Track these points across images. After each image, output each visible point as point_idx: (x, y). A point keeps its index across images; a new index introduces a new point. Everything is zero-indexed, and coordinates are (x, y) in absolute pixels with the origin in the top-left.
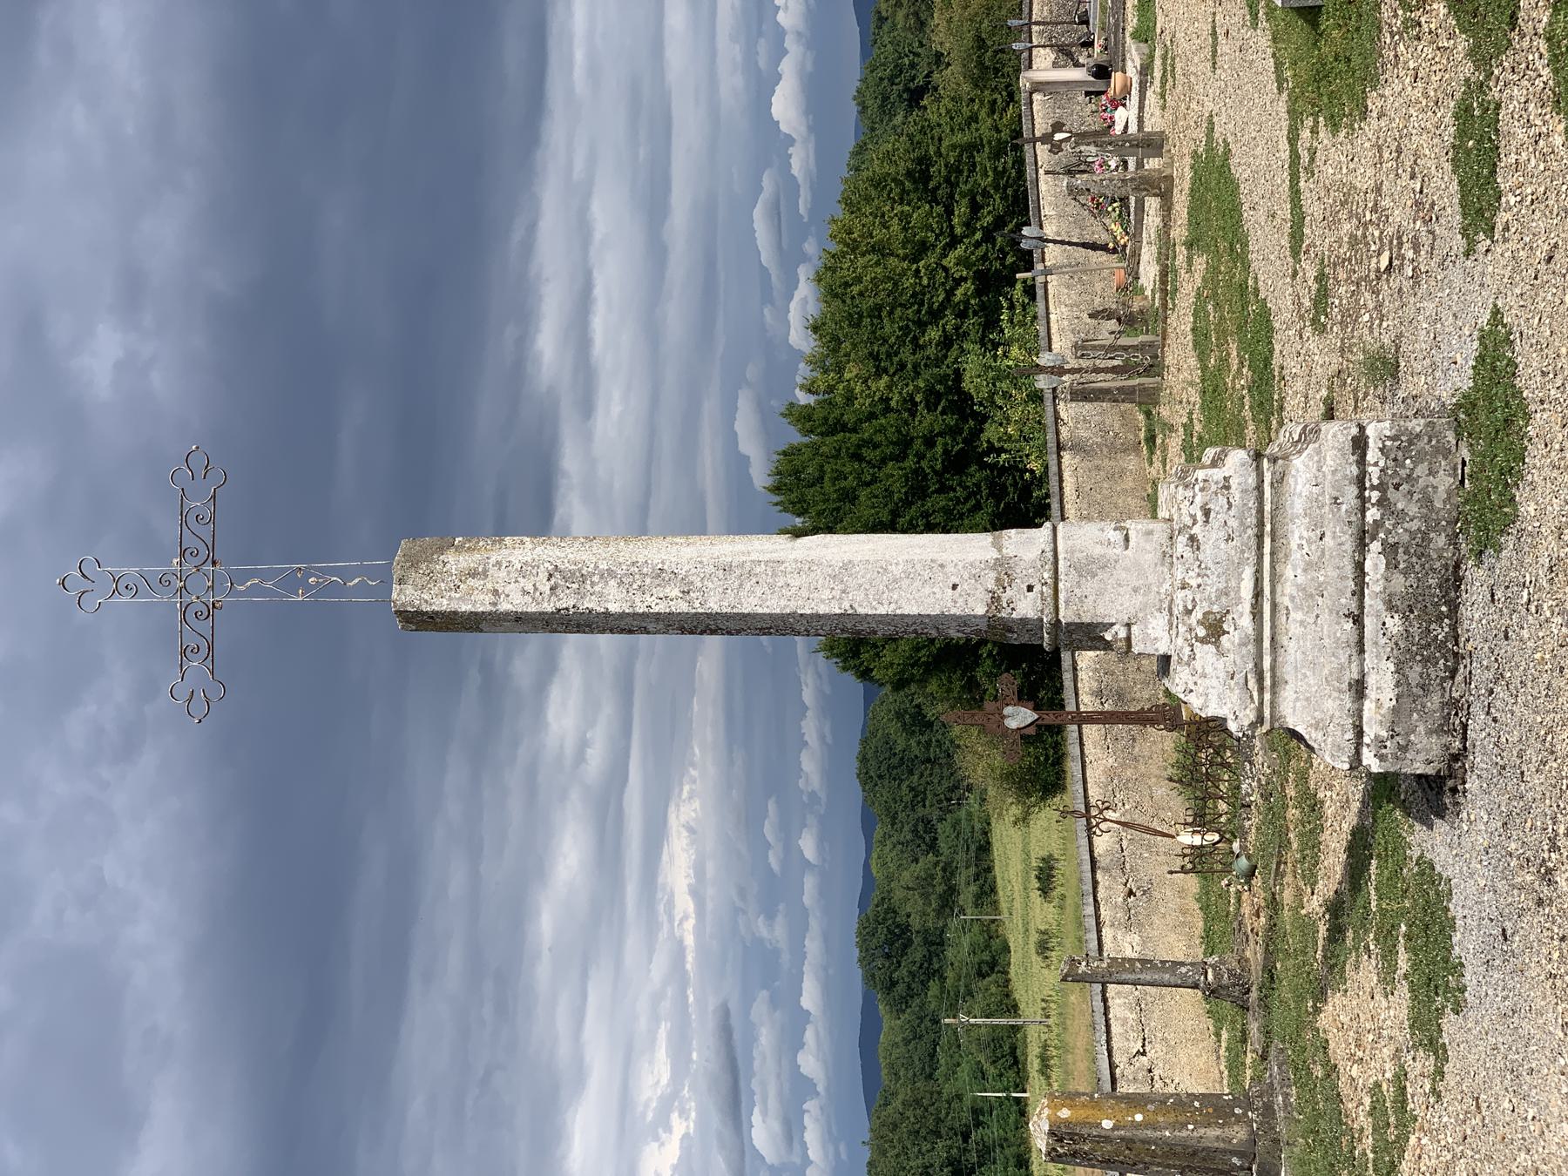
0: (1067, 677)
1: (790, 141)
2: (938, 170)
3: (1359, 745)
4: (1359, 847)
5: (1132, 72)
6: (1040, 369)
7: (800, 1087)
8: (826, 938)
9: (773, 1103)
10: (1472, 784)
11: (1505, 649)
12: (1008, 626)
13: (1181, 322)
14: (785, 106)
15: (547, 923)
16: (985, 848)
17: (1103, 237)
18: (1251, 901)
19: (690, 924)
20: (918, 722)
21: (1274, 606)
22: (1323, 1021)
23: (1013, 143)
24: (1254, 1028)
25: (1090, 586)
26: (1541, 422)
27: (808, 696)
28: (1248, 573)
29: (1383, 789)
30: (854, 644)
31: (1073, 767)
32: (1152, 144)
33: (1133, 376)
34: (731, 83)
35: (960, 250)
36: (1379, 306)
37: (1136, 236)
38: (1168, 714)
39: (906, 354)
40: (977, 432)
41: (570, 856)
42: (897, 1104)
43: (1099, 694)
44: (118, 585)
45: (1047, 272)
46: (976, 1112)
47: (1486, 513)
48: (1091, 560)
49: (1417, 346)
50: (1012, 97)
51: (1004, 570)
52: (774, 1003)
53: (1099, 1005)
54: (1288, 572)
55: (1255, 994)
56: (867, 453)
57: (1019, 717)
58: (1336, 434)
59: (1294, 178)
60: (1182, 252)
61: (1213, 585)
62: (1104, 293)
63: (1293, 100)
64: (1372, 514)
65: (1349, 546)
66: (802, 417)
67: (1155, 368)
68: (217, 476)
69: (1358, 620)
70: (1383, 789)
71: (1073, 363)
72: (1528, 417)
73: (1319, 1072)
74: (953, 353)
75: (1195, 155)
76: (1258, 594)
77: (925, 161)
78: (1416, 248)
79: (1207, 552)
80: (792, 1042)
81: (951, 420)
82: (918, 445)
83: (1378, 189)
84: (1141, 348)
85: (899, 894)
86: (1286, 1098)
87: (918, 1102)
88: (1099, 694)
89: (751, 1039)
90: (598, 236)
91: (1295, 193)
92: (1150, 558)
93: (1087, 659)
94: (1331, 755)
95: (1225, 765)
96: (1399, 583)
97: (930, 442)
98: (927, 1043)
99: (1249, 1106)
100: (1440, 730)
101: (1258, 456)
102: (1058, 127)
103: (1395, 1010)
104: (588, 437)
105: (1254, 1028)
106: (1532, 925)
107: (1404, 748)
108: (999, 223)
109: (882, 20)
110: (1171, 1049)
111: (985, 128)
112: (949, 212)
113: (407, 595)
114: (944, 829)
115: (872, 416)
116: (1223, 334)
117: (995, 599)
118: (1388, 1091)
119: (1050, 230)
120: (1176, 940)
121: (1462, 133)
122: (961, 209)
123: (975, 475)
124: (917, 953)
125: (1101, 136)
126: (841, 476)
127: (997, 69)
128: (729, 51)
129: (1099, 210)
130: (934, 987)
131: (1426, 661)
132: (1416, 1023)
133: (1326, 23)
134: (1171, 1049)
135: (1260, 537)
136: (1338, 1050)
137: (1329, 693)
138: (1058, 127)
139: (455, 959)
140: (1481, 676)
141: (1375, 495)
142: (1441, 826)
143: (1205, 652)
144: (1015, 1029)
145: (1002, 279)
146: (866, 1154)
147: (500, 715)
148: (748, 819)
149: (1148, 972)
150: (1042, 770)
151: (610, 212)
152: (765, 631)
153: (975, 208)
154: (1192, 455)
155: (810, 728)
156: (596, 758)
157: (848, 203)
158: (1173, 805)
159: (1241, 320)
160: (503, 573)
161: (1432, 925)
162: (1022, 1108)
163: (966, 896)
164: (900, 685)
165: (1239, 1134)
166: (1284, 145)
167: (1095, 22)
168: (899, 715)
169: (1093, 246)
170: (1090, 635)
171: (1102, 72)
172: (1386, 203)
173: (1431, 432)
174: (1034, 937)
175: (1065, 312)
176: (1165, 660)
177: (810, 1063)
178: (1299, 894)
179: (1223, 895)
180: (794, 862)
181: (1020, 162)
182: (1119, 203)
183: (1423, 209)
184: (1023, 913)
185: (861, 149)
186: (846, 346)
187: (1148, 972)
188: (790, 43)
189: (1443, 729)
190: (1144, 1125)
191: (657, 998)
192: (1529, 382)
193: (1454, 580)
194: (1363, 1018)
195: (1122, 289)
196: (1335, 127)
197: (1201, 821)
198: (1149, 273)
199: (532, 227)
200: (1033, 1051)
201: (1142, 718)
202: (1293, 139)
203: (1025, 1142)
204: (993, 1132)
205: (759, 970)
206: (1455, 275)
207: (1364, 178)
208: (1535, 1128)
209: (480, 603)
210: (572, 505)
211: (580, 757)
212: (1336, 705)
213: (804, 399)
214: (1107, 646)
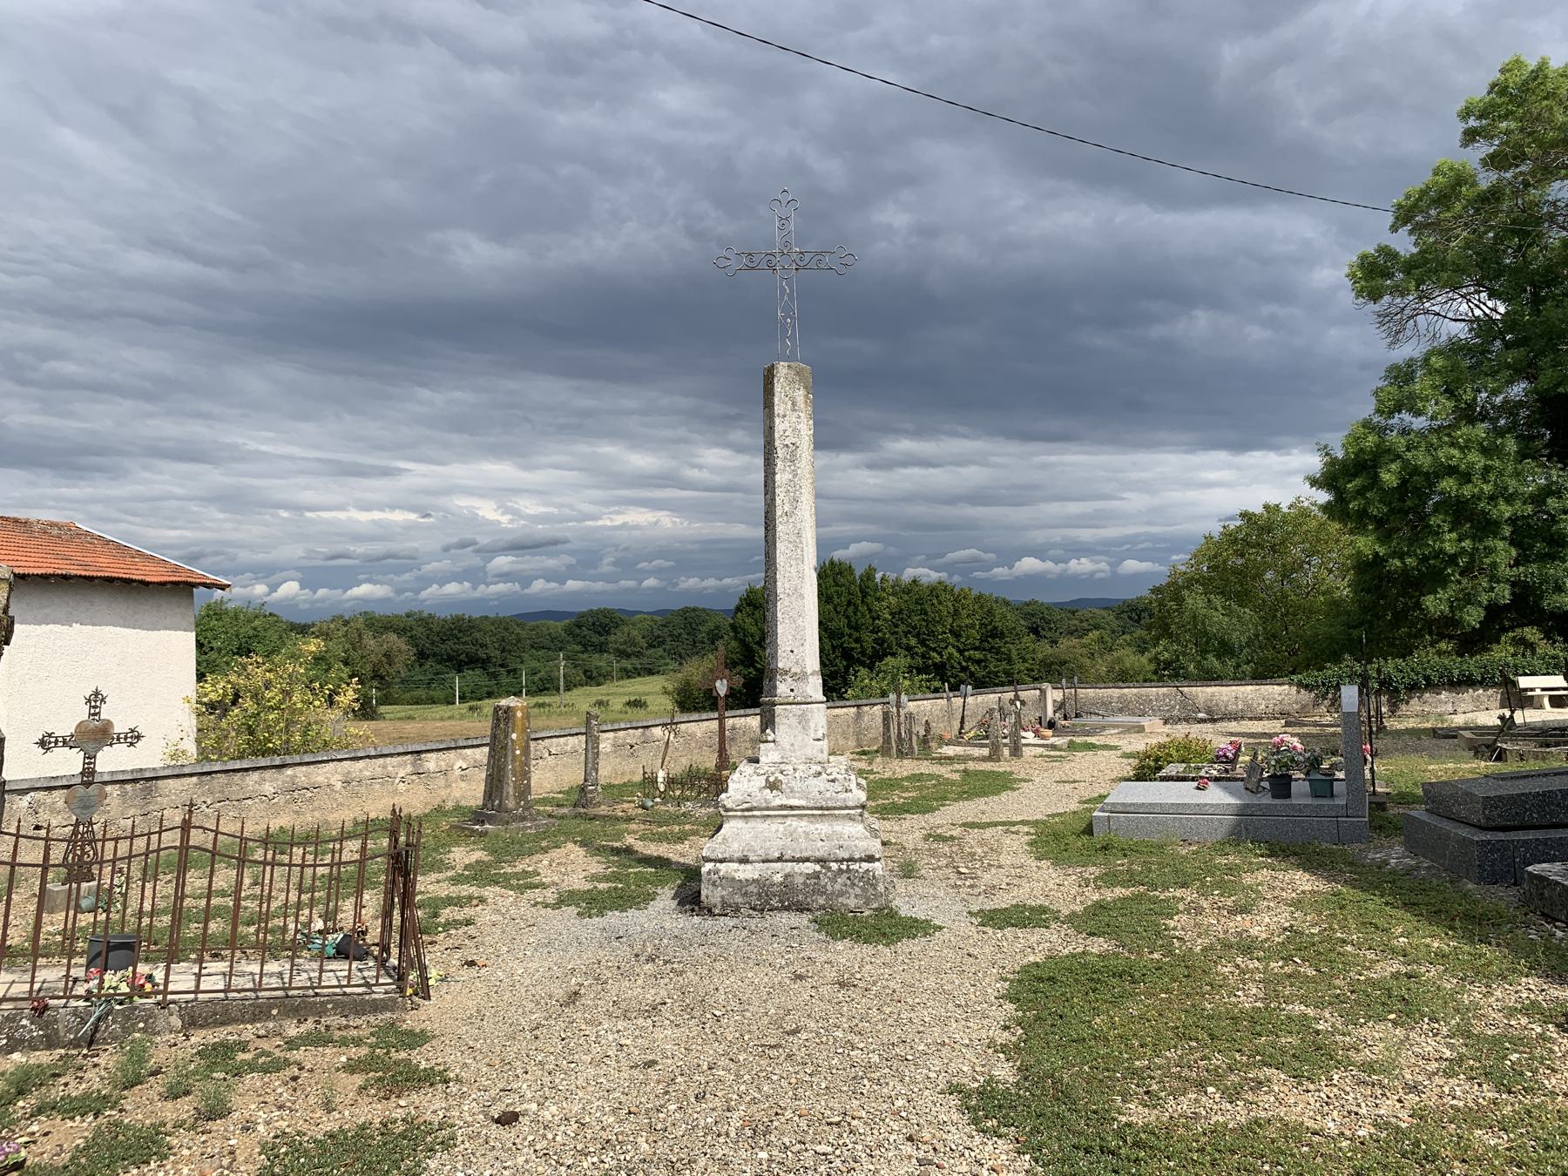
0: (742, 712)
1: (1011, 567)
2: (997, 642)
3: (715, 861)
4: (661, 862)
5: (1053, 740)
6: (899, 696)
7: (526, 581)
8: (603, 592)
9: (519, 567)
10: (696, 919)
11: (767, 935)
12: (772, 679)
13: (925, 767)
14: (1029, 564)
15: (608, 450)
16: (651, 672)
17: (967, 727)
18: (630, 808)
19: (608, 523)
20: (714, 637)
21: (786, 816)
22: (570, 845)
23: (1011, 681)
24: (565, 811)
25: (794, 721)
26: (885, 952)
27: (727, 581)
28: (803, 803)
29: (692, 874)
30: (758, 606)
31: (695, 716)
32: (1016, 751)
33: (897, 743)
34: (1039, 536)
35: (956, 654)
36: (940, 868)
37: (968, 744)
38: (725, 763)
39: (902, 628)
40: (863, 664)
41: (642, 461)
42: (518, 630)
43: (733, 728)
44: (784, 220)
45: (949, 699)
46: (515, 670)
47: (836, 924)
48: (807, 721)
49: (920, 887)
50: (1035, 679)
51: (801, 677)
52: (570, 566)
53: (574, 731)
54: (803, 823)
55: (582, 810)
56: (851, 609)
57: (722, 688)
58: (875, 847)
59: (1003, 824)
60: (962, 767)
61: (797, 785)
62: (938, 728)
63: (1044, 823)
64: (834, 866)
65: (818, 854)
66: (869, 575)
67: (901, 755)
68: (842, 270)
69: (779, 859)
70: (692, 874)
71: (902, 712)
72: (887, 945)
73: (544, 844)
74: (904, 652)
75: (1012, 773)
76: (792, 808)
77: (1002, 635)
78: (971, 886)
79: (812, 781)
80: (550, 576)
81: (869, 651)
82: (856, 634)
83: (1000, 867)
84: (911, 747)
85: (626, 629)
86: (529, 827)
87: (519, 641)
88: (733, 728)
89: (550, 555)
90: (960, 470)
91: (996, 824)
92: (809, 753)
93: (754, 722)
94: (710, 847)
95: (699, 793)
96: (799, 880)
97: (857, 640)
98: (552, 645)
99: (525, 809)
100: (723, 902)
101: (863, 807)
102: (1023, 703)
103: (578, 882)
104: (857, 467)
105: (565, 811)
106: (624, 951)
107: (714, 884)
108: (972, 675)
109: (1073, 613)
110: (552, 769)
111: (1019, 666)
112: (976, 649)
113: (782, 369)
114: (660, 651)
115: (870, 611)
116: (920, 789)
117: (786, 672)
118: (536, 880)
119: (970, 700)
120: (607, 771)
121: (1032, 909)
122: (978, 655)
123: (841, 664)
124: (596, 639)
125: (1019, 726)
126: (839, 595)
127: (1051, 671)
128: (1057, 535)
129: (981, 725)
130: (579, 648)
131: (759, 894)
132: (572, 893)
133: (1085, 838)
134: (552, 769)
135: (821, 808)
136: (555, 853)
137: (742, 845)
138: (1023, 703)
139: (590, 403)
140: (752, 923)
141: (844, 867)
142: (674, 904)
143: (761, 781)
144: (558, 690)
145: (943, 676)
146: (492, 615)
147: (716, 425)
148: (663, 552)
149: (592, 756)
150: (693, 701)
151: (973, 476)
152: (767, 555)
153: (978, 662)
154: (860, 773)
155: (711, 582)
156: (693, 474)
157: (979, 598)
158: (678, 767)
159: (928, 798)
160: (794, 420)
161: (623, 900)
162: (518, 694)
163: (627, 664)
164: (734, 627)
165: (511, 804)
166: (1020, 818)
167: (1077, 721)
168: (717, 628)
169: (962, 722)
170: (768, 722)
171: (1051, 725)
172: (993, 871)
173: (877, 896)
174: (605, 699)
175: (928, 708)
176: (757, 761)
177: (538, 585)
178: (634, 832)
179: (632, 794)
180: (643, 575)
181: (1003, 685)
182: (986, 733)
183: (991, 890)
184: (618, 692)
185: (1007, 603)
186: (906, 597)
187: (592, 756)
188: (1061, 566)
189: (725, 904)
190: (514, 756)
191: (571, 507)
192: (905, 946)
193: (801, 908)
194: (573, 866)
195: (941, 738)
196: (1030, 844)
197: (670, 782)
198: (949, 751)
199: (965, 436)
200: (547, 699)
201: (722, 751)
202: (1023, 823)
203: (500, 696)
204: (505, 680)
205: (587, 560)
206: (959, 907)
207: (1005, 859)
208: (521, 955)
209: (780, 407)
210: (825, 458)
211: (693, 466)
212: (735, 849)
213: (878, 576)
214: (763, 731)
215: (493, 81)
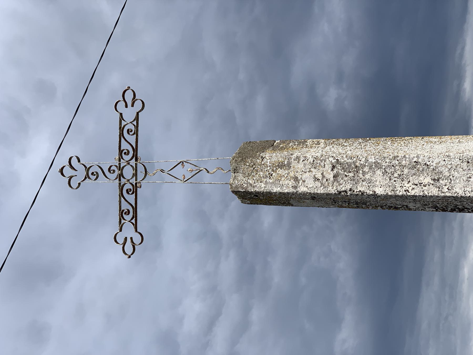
139: (436, 280)
199: (463, 49)
215: (257, 315)
